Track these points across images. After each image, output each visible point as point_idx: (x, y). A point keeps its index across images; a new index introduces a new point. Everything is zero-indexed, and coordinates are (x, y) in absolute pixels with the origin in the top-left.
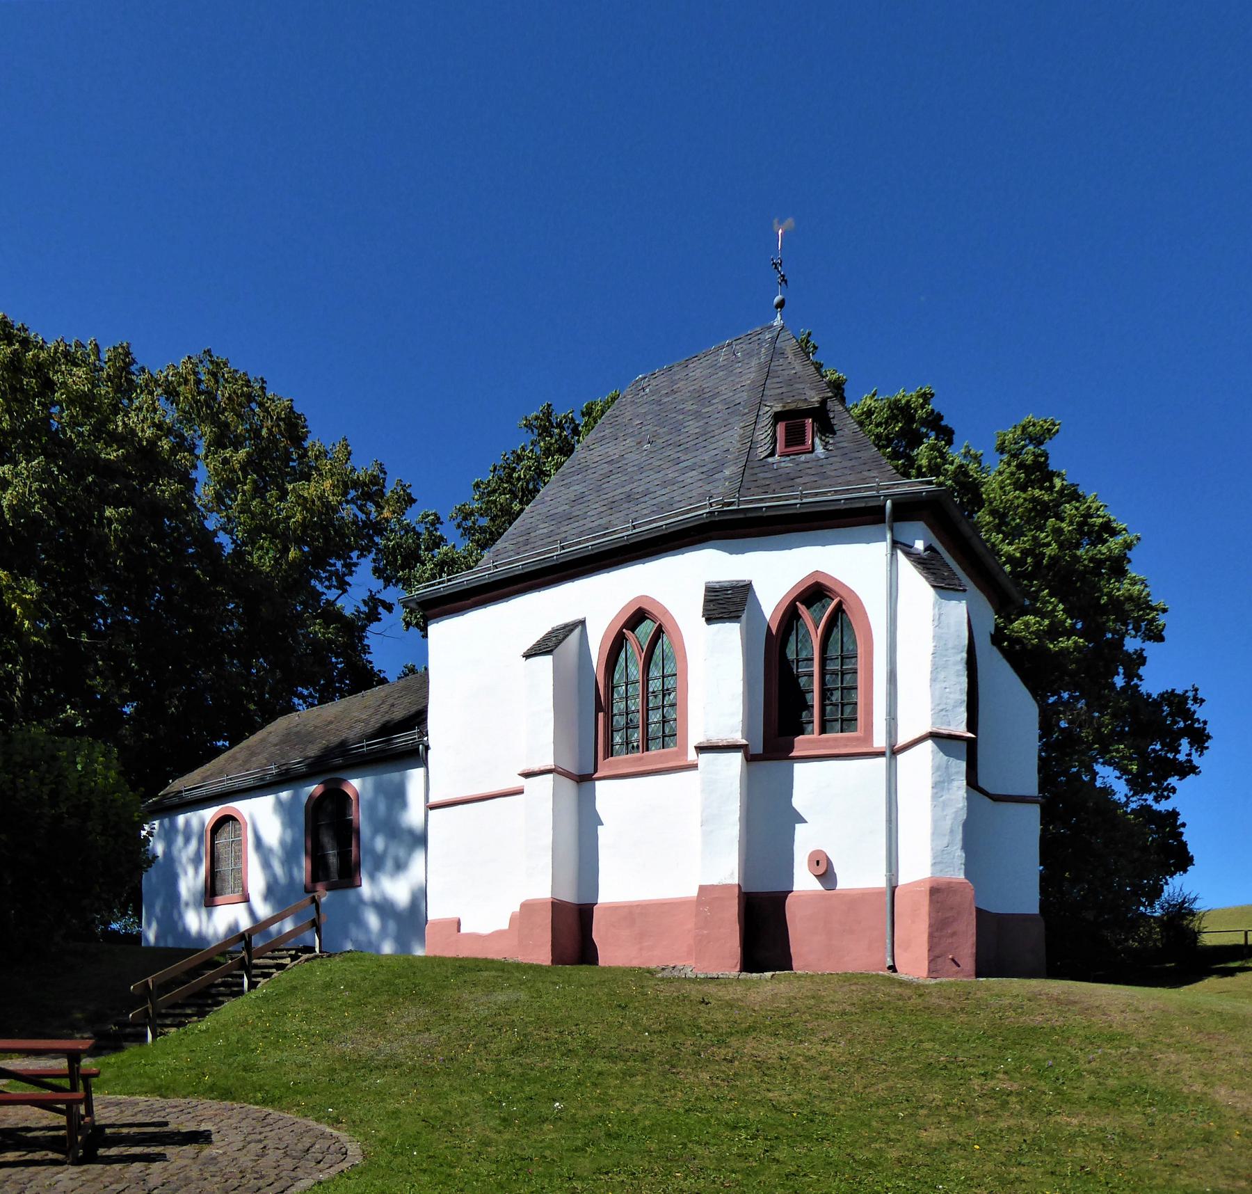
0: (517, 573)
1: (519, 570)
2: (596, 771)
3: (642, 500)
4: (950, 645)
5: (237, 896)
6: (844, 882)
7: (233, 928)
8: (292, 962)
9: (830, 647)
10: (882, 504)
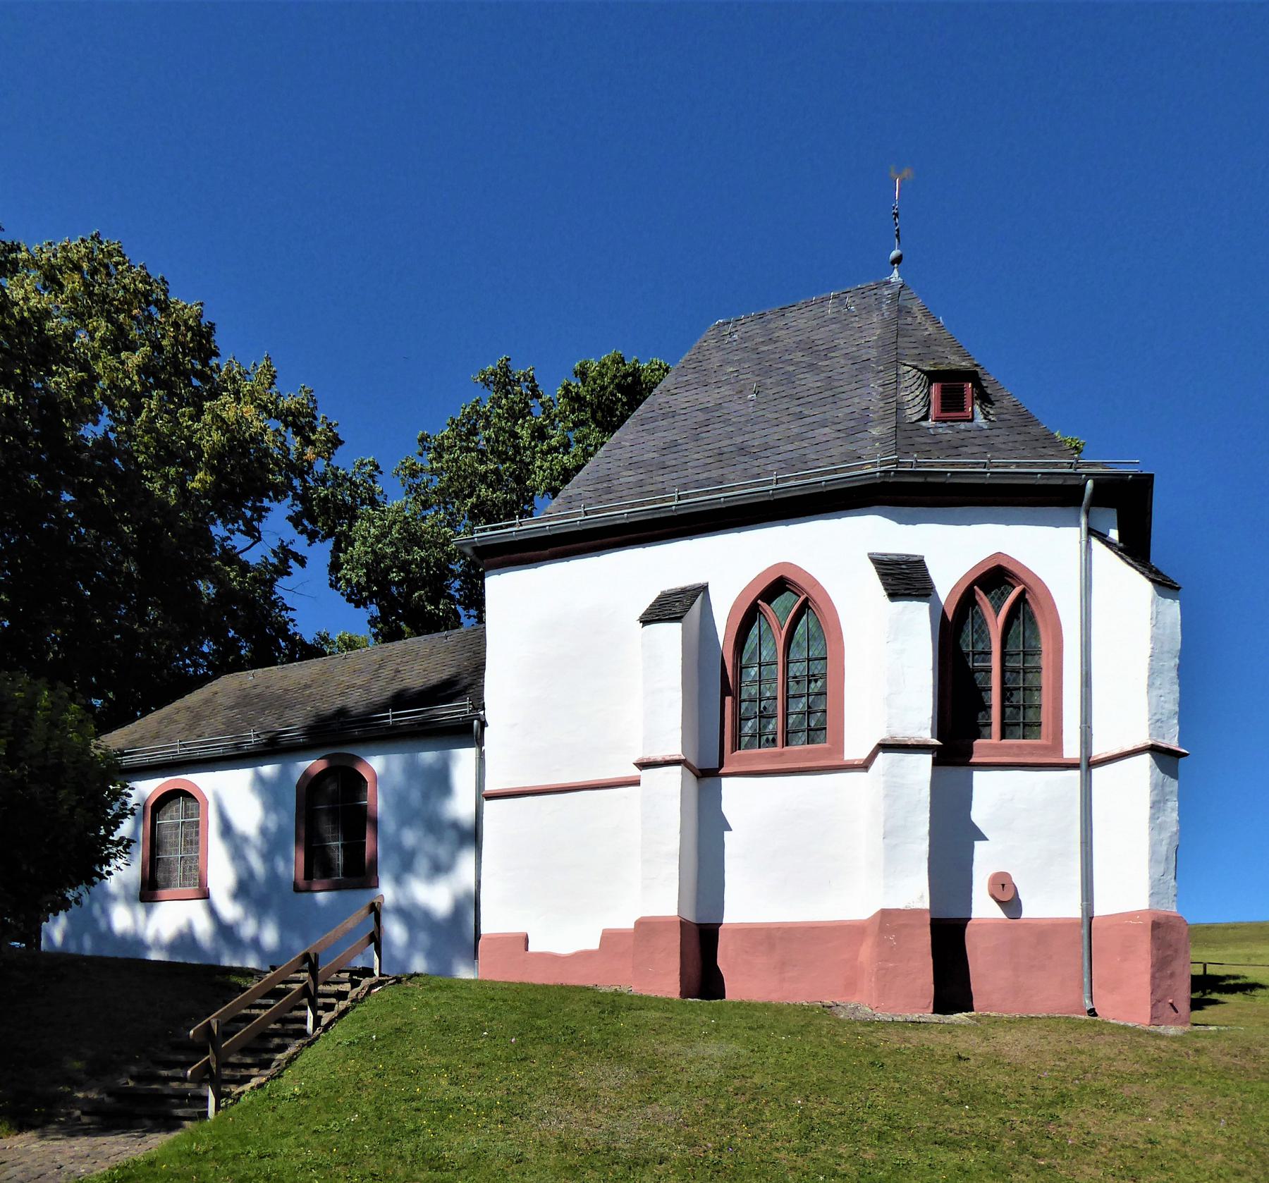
0: (618, 522)
1: (623, 518)
2: (721, 765)
3: (762, 454)
4: (1166, 649)
5: (191, 890)
6: (1031, 910)
7: (186, 940)
8: (352, 988)
9: (1010, 642)
10: (1082, 483)
